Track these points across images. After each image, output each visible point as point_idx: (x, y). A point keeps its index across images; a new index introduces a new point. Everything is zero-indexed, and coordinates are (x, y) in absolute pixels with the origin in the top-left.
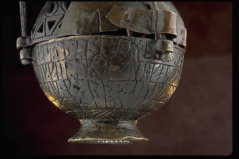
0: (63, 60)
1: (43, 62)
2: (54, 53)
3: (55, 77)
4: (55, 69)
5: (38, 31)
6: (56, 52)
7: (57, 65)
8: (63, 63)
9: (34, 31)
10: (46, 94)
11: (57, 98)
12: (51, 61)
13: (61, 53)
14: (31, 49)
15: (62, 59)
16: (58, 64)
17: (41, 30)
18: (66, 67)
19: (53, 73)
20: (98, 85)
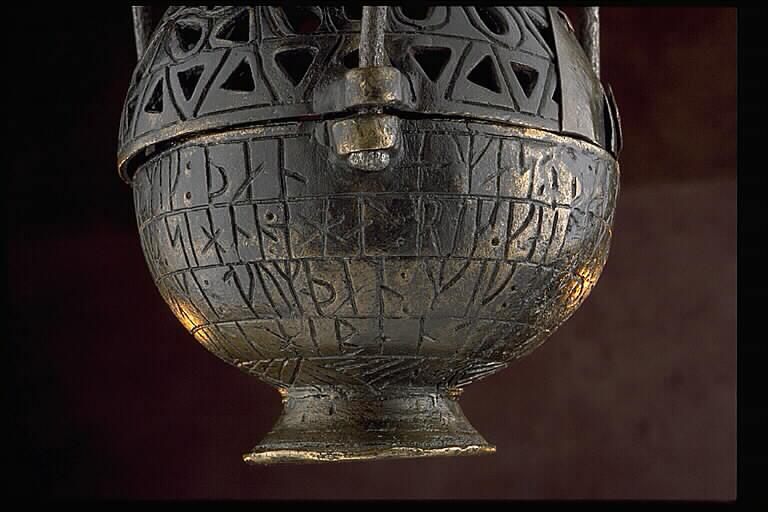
0: (567, 206)
1: (491, 189)
2: (544, 175)
3: (524, 249)
4: (536, 226)
5: (148, 109)
6: (550, 174)
7: (547, 216)
8: (564, 213)
9: (537, 27)
10: (174, 307)
11: (212, 317)
12: (529, 196)
13: (566, 182)
14: (596, 91)
15: (565, 202)
16: (549, 213)
17: (156, 106)
18: (569, 229)
19: (520, 237)
20: (333, 294)
